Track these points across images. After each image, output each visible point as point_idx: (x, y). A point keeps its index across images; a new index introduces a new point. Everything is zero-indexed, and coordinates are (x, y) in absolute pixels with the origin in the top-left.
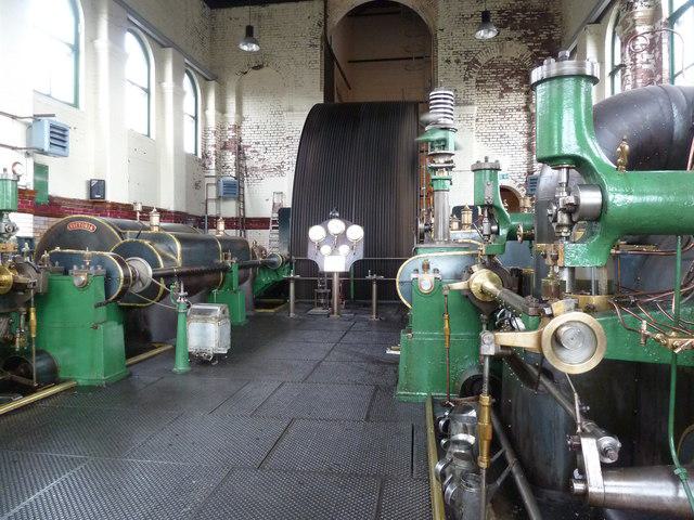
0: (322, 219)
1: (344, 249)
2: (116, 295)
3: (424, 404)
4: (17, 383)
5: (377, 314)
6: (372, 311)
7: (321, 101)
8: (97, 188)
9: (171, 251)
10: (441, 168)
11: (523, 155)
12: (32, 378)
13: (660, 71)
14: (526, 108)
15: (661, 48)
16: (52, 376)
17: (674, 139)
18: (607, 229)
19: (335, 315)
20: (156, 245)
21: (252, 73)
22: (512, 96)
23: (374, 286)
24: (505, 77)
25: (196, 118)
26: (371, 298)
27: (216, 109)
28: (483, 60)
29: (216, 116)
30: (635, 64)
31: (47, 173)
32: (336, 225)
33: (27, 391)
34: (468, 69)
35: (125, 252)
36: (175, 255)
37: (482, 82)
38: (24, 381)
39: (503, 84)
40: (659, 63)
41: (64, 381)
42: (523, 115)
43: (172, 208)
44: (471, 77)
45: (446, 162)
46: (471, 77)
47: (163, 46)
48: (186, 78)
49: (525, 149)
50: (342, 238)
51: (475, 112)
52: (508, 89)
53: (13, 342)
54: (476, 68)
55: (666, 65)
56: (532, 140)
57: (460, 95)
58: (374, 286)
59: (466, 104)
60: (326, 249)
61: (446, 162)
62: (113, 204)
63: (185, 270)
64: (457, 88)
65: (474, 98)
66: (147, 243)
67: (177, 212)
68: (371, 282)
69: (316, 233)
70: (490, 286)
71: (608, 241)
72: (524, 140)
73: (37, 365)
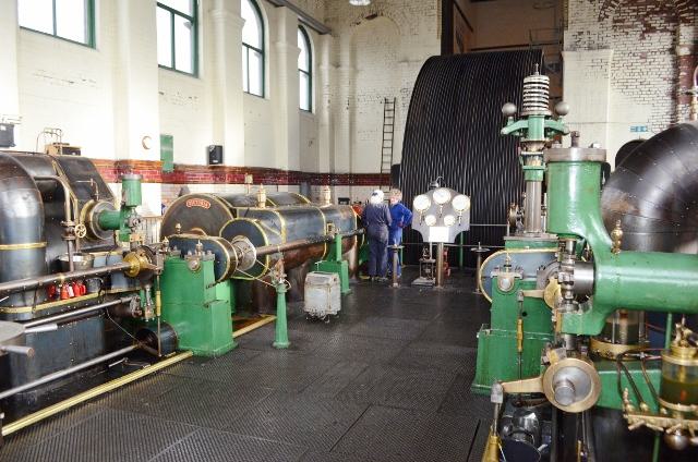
1: (449, 220)
4: (147, 352)
7: (438, 52)
8: (215, 154)
9: (274, 226)
12: (157, 349)
14: (672, 51)
16: (174, 346)
17: (663, 230)
18: (599, 306)
19: (439, 286)
20: (263, 223)
21: (365, 23)
22: (655, 37)
24: (647, 15)
27: (330, 63)
29: (330, 70)
31: (172, 144)
32: (442, 195)
33: (154, 360)
34: (603, 9)
35: (229, 234)
36: (280, 230)
38: (150, 349)
39: (646, 25)
41: (184, 351)
42: (668, 59)
43: (286, 168)
44: (607, 17)
46: (607, 17)
48: (300, 34)
49: (669, 98)
50: (448, 207)
51: (611, 56)
52: (650, 29)
53: (143, 315)
54: (613, 6)
56: (678, 87)
57: (594, 38)
59: (601, 47)
60: (430, 219)
62: (230, 168)
63: (287, 246)
64: (590, 29)
65: (610, 40)
66: (254, 221)
67: (291, 172)
72: (667, 87)
73: (162, 336)
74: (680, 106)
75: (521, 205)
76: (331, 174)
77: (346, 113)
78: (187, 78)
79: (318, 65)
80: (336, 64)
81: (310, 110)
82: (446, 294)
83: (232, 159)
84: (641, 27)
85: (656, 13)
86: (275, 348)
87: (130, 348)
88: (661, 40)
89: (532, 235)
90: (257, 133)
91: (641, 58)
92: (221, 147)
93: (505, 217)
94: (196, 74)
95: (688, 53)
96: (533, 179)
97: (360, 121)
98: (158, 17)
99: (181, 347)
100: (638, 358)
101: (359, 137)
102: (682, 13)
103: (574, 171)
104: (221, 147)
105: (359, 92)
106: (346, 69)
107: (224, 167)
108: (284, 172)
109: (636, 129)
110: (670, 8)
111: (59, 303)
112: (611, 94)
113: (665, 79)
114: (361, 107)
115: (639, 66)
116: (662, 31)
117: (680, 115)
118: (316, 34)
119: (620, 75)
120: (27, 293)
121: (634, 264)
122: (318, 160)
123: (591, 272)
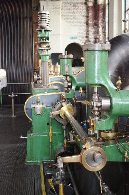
3: (39, 166)
5: (14, 114)
6: (12, 112)
10: (44, 49)
11: (84, 27)
23: (13, 100)
26: (11, 103)
42: (84, 7)
45: (47, 47)
49: (85, 25)
51: (61, 4)
58: (13, 100)
61: (47, 47)
68: (11, 98)
70: (67, 113)
71: (113, 120)
72: (84, 20)
74: (90, 28)
75: (38, 72)
89: (46, 87)
91: (74, 6)
93: (32, 77)
100: (122, 138)
103: (97, 55)
112: (62, 22)
113: (83, 16)
117: (90, 32)
120: (112, 139)
123: (109, 101)
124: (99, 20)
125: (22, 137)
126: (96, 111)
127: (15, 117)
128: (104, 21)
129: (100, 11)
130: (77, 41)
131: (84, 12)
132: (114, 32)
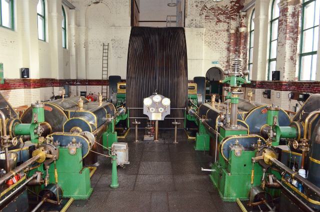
0: (149, 94)
2: (86, 155)
8: (25, 72)
11: (225, 53)
13: (297, 27)
15: (298, 18)
16: (68, 199)
22: (221, 24)
24: (218, 15)
25: (65, 29)
28: (209, 6)
30: (287, 23)
32: (157, 98)
34: (201, 10)
37: (208, 16)
39: (218, 19)
40: (297, 24)
42: (226, 34)
43: (58, 78)
45: (238, 91)
47: (70, 9)
52: (219, 21)
54: (205, 10)
55: (300, 25)
57: (198, 23)
62: (33, 80)
67: (60, 80)
69: (147, 102)
70: (272, 159)
72: (226, 45)
74: (231, 54)
76: (76, 80)
77: (83, 50)
78: (8, 30)
79: (69, 25)
80: (78, 25)
81: (65, 48)
82: (160, 144)
83: (34, 75)
84: (216, 20)
85: (222, 14)
86: (111, 188)
87: (41, 203)
88: (223, 26)
90: (45, 62)
92: (28, 69)
94: (13, 28)
95: (234, 32)
96: (234, 103)
97: (91, 54)
98: (261, 89)
99: (65, 196)
101: (90, 62)
102: (232, 15)
103: (153, 114)
104: (28, 69)
105: (89, 39)
106: (83, 28)
107: (30, 80)
108: (57, 80)
109: (213, 63)
110: (227, 13)
111: (11, 188)
112: (204, 47)
113: (225, 42)
114: (91, 47)
115: (215, 35)
116: (224, 22)
118: (68, 9)
119: (207, 39)
121: (42, 67)
122: (70, 72)
124: (240, 47)
125: (203, 170)
126: (153, 101)
127: (275, 207)
128: (245, 48)
129: (242, 39)
130: (218, 66)
131: (226, 39)
132: (259, 60)
